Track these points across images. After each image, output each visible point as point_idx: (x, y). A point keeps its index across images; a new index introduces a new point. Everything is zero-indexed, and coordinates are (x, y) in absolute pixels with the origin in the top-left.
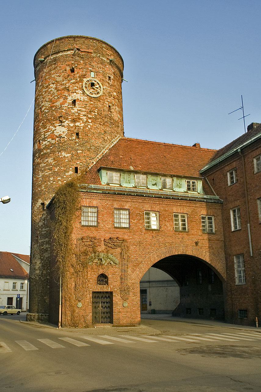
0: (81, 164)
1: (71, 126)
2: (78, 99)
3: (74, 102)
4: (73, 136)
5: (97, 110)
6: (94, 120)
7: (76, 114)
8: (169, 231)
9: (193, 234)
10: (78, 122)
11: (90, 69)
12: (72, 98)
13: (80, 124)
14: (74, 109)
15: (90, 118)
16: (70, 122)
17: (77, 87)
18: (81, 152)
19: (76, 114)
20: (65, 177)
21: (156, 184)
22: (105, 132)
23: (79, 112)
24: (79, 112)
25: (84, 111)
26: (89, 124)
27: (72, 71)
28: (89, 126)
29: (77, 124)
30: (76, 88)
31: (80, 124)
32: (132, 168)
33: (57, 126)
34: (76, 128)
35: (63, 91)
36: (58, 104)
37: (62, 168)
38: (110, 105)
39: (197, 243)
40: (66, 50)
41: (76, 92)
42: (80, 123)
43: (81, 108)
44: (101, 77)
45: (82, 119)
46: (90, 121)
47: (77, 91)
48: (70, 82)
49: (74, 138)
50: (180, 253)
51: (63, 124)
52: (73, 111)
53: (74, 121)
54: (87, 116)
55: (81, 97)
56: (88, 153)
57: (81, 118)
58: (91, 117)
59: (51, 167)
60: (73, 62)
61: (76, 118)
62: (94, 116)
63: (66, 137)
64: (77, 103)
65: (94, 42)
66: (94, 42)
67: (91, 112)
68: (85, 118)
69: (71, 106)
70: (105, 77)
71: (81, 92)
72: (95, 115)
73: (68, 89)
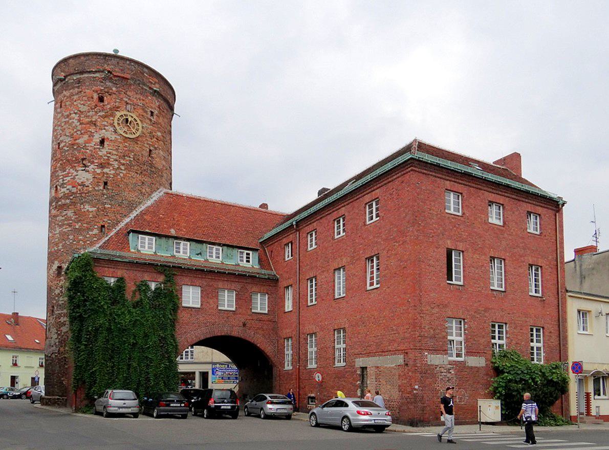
1: (98, 172)
3: (102, 142)
5: (133, 154)
6: (129, 167)
7: (104, 157)
8: (212, 308)
9: (240, 314)
10: (107, 168)
11: (125, 99)
12: (100, 136)
15: (123, 164)
16: (96, 167)
17: (107, 122)
18: (110, 206)
19: (104, 157)
21: (200, 254)
22: (143, 183)
23: (109, 155)
24: (109, 155)
26: (121, 171)
27: (101, 99)
29: (106, 170)
30: (106, 123)
31: (110, 171)
32: (173, 232)
34: (103, 175)
35: (88, 125)
36: (81, 141)
38: (152, 148)
39: (244, 325)
41: (105, 129)
42: (109, 170)
43: (111, 151)
44: (140, 111)
46: (123, 167)
47: (106, 128)
49: (101, 188)
50: (223, 334)
51: (87, 168)
52: (100, 154)
53: (102, 166)
56: (119, 208)
58: (125, 162)
59: (71, 222)
60: (103, 88)
62: (128, 162)
63: (91, 186)
64: (106, 143)
65: (132, 64)
66: (132, 64)
67: (124, 156)
68: (116, 164)
69: (99, 147)
70: (146, 112)
71: (112, 129)
73: (95, 124)
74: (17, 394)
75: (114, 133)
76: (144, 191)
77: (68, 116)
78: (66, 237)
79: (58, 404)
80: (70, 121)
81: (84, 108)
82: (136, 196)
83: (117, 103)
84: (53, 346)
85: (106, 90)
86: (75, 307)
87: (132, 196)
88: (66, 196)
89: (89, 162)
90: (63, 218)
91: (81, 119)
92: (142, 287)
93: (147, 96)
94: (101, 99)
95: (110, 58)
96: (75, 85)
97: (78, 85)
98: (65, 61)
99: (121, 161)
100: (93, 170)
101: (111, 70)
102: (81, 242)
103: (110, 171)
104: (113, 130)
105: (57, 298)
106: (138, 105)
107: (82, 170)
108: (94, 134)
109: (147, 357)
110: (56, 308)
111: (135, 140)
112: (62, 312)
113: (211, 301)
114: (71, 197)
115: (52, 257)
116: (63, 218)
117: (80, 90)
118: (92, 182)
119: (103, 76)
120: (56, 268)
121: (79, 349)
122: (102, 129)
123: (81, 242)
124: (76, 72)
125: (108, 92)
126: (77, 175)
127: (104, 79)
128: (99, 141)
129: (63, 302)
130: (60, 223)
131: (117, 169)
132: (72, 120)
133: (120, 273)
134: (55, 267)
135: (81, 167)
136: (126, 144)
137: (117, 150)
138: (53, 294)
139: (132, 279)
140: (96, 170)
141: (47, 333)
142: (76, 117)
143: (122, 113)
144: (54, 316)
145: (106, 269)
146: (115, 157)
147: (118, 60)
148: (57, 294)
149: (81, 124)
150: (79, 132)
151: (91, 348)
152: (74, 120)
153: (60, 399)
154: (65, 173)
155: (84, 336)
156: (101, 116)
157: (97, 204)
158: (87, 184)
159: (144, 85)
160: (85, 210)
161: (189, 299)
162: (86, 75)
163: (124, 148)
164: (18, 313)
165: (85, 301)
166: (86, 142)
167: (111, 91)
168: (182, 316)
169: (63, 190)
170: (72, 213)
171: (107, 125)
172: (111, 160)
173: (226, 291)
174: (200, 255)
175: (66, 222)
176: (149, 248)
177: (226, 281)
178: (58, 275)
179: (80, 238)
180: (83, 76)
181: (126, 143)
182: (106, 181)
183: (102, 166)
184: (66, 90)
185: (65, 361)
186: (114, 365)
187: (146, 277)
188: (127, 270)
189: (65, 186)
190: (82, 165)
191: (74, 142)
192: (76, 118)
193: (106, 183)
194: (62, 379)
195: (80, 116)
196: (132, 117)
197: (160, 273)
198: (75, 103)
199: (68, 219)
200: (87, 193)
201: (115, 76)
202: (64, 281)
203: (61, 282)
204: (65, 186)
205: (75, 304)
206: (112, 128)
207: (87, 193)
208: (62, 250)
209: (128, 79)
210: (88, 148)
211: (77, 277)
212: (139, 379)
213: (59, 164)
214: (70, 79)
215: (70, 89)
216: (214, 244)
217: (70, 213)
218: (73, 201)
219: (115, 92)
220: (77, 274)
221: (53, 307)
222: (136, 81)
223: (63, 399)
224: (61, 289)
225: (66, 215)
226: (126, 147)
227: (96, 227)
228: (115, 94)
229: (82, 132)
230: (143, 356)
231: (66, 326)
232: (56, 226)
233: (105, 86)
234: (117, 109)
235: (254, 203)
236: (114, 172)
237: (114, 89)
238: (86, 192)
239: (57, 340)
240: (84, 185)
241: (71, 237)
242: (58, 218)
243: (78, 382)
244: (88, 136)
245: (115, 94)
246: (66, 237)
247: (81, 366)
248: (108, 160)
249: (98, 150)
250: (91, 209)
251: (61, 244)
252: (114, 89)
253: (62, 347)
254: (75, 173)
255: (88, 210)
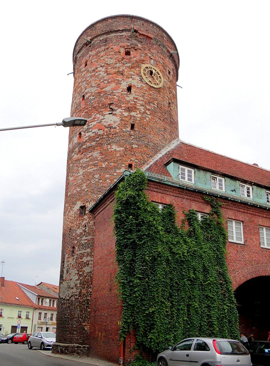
0: (136, 161)
1: (125, 115)
2: (134, 86)
3: (129, 89)
4: (127, 127)
6: (153, 113)
7: (131, 102)
12: (127, 84)
13: (137, 114)
14: (129, 96)
15: (149, 110)
16: (123, 110)
17: (134, 72)
18: (137, 146)
19: (131, 102)
20: (115, 174)
21: (234, 190)
23: (135, 100)
24: (135, 100)
25: (141, 100)
27: (128, 53)
28: (147, 119)
29: (133, 114)
30: (132, 73)
33: (106, 114)
34: (131, 118)
37: (112, 164)
40: (121, 29)
45: (139, 109)
46: (148, 112)
48: (125, 66)
49: (129, 129)
51: (114, 112)
52: (128, 99)
54: (145, 106)
55: (138, 84)
56: (145, 149)
57: (137, 107)
58: (150, 108)
61: (131, 107)
62: (153, 109)
63: (118, 128)
64: (133, 90)
66: (155, 27)
71: (138, 78)
72: (155, 107)
74: (4, 339)
75: (140, 82)
76: (166, 136)
77: (94, 71)
78: (91, 177)
79: (78, 353)
80: (97, 74)
81: (109, 61)
82: (160, 140)
83: (142, 57)
84: (72, 288)
85: (132, 46)
86: (125, 232)
87: (157, 139)
88: (91, 139)
89: (116, 107)
90: (88, 160)
91: (108, 70)
92: (190, 218)
93: (166, 58)
94: (128, 53)
95: (135, 20)
96: (101, 44)
97: (104, 44)
98: (92, 26)
99: (147, 107)
100: (120, 114)
101: (137, 29)
102: (107, 180)
103: (137, 114)
104: (139, 79)
105: (78, 238)
106: (160, 62)
107: (109, 114)
108: (122, 82)
109: (207, 296)
110: (77, 248)
111: (159, 90)
112: (85, 251)
113: (254, 237)
114: (98, 139)
115: (69, 200)
116: (88, 160)
117: (107, 47)
118: (118, 124)
119: (130, 34)
120: (79, 208)
121: (131, 284)
122: (129, 78)
123: (107, 180)
124: (104, 32)
125: (134, 48)
126: (104, 119)
127: (131, 37)
128: (126, 88)
129: (86, 241)
130: (84, 165)
131: (143, 113)
132: (99, 73)
133: (168, 200)
134: (77, 207)
135: (109, 111)
136: (151, 92)
137: (143, 96)
138: (74, 234)
139: (182, 207)
140: (124, 113)
141: (64, 275)
142: (103, 69)
143: (148, 65)
144: (75, 257)
145: (155, 193)
146: (141, 102)
147: (143, 22)
148: (79, 233)
149: (108, 74)
150: (106, 82)
151: (147, 282)
152: (101, 73)
153: (80, 347)
154: (90, 119)
155: (138, 266)
156: (129, 67)
157: (124, 145)
158: (114, 125)
159: (164, 47)
160: (113, 150)
161: (233, 234)
162: (113, 35)
163: (150, 96)
164: (4, 278)
165: (138, 225)
166: (113, 89)
167: (137, 47)
168: (230, 253)
169: (87, 135)
170: (98, 153)
171: (133, 74)
172: (138, 104)
173: (264, 229)
174: (234, 192)
175: (91, 163)
176: (189, 180)
177: (265, 217)
178: (81, 213)
179: (106, 176)
180: (110, 35)
181: (151, 91)
182: (132, 123)
183: (129, 110)
184: (91, 51)
185: (88, 303)
186: (173, 304)
187: (194, 207)
188: (176, 197)
189: (90, 130)
190: (109, 109)
191: (100, 90)
192: (103, 70)
193: (133, 127)
194: (84, 324)
195: (107, 68)
196: (156, 71)
197: (207, 203)
198: (102, 58)
199: (93, 159)
200: (114, 134)
201: (140, 34)
202: (88, 220)
203: (85, 222)
204: (90, 130)
205: (126, 229)
206: (139, 77)
207: (114, 134)
208: (87, 190)
209: (151, 38)
210: (116, 94)
211: (130, 197)
212: (200, 323)
213: (84, 113)
214: (96, 41)
215: (97, 49)
216: (245, 182)
217: (96, 154)
218: (100, 142)
219: (140, 48)
220: (130, 192)
221: (74, 247)
222: (157, 41)
223: (85, 347)
224: (84, 229)
225: (92, 156)
226: (150, 94)
227: (124, 165)
228: (141, 49)
229: (110, 81)
230: (204, 295)
231: (90, 265)
232: (80, 168)
233: (131, 43)
234: (143, 62)
235: (251, 163)
236: (141, 116)
237: (139, 45)
238: (113, 133)
239: (79, 282)
240: (111, 128)
241: (97, 176)
242: (81, 161)
243: (128, 326)
244: (115, 84)
245: (141, 49)
246: (91, 177)
247: (133, 306)
248: (135, 104)
249: (125, 95)
250: (118, 149)
251: (85, 184)
252: (139, 45)
253: (84, 288)
254: (102, 117)
255: (115, 150)
